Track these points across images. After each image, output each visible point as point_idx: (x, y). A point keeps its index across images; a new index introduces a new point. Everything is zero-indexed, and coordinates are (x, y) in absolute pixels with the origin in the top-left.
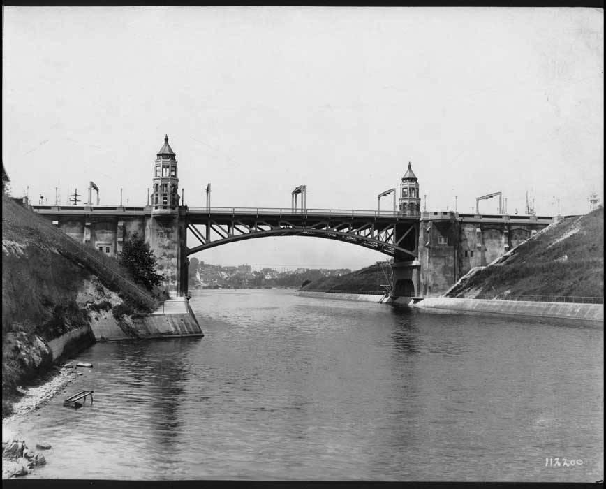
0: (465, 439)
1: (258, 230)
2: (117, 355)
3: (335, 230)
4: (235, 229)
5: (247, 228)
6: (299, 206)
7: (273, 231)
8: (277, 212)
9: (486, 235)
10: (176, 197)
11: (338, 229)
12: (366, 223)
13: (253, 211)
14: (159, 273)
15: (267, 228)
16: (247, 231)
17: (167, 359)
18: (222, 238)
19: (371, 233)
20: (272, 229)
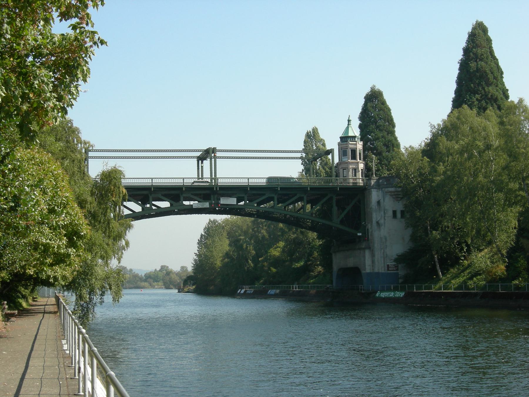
0: (411, 345)
1: (154, 208)
2: (51, 21)
3: (256, 205)
4: (122, 208)
5: (139, 204)
6: (207, 174)
7: (173, 208)
8: (178, 182)
9: (59, 216)
10: (161, 275)
11: (259, 204)
12: (295, 195)
13: (147, 182)
14: (88, 227)
15: (165, 204)
16: (137, 208)
17: (5, 92)
18: (132, 213)
19: (303, 207)
20: (171, 205)
